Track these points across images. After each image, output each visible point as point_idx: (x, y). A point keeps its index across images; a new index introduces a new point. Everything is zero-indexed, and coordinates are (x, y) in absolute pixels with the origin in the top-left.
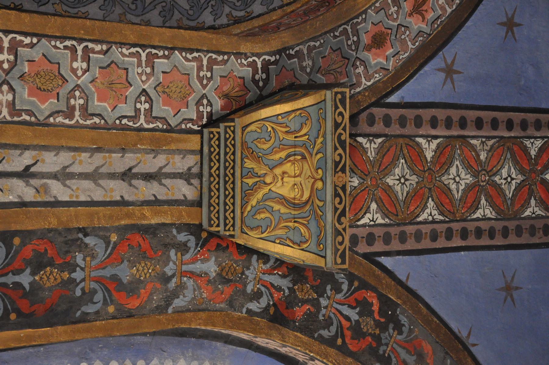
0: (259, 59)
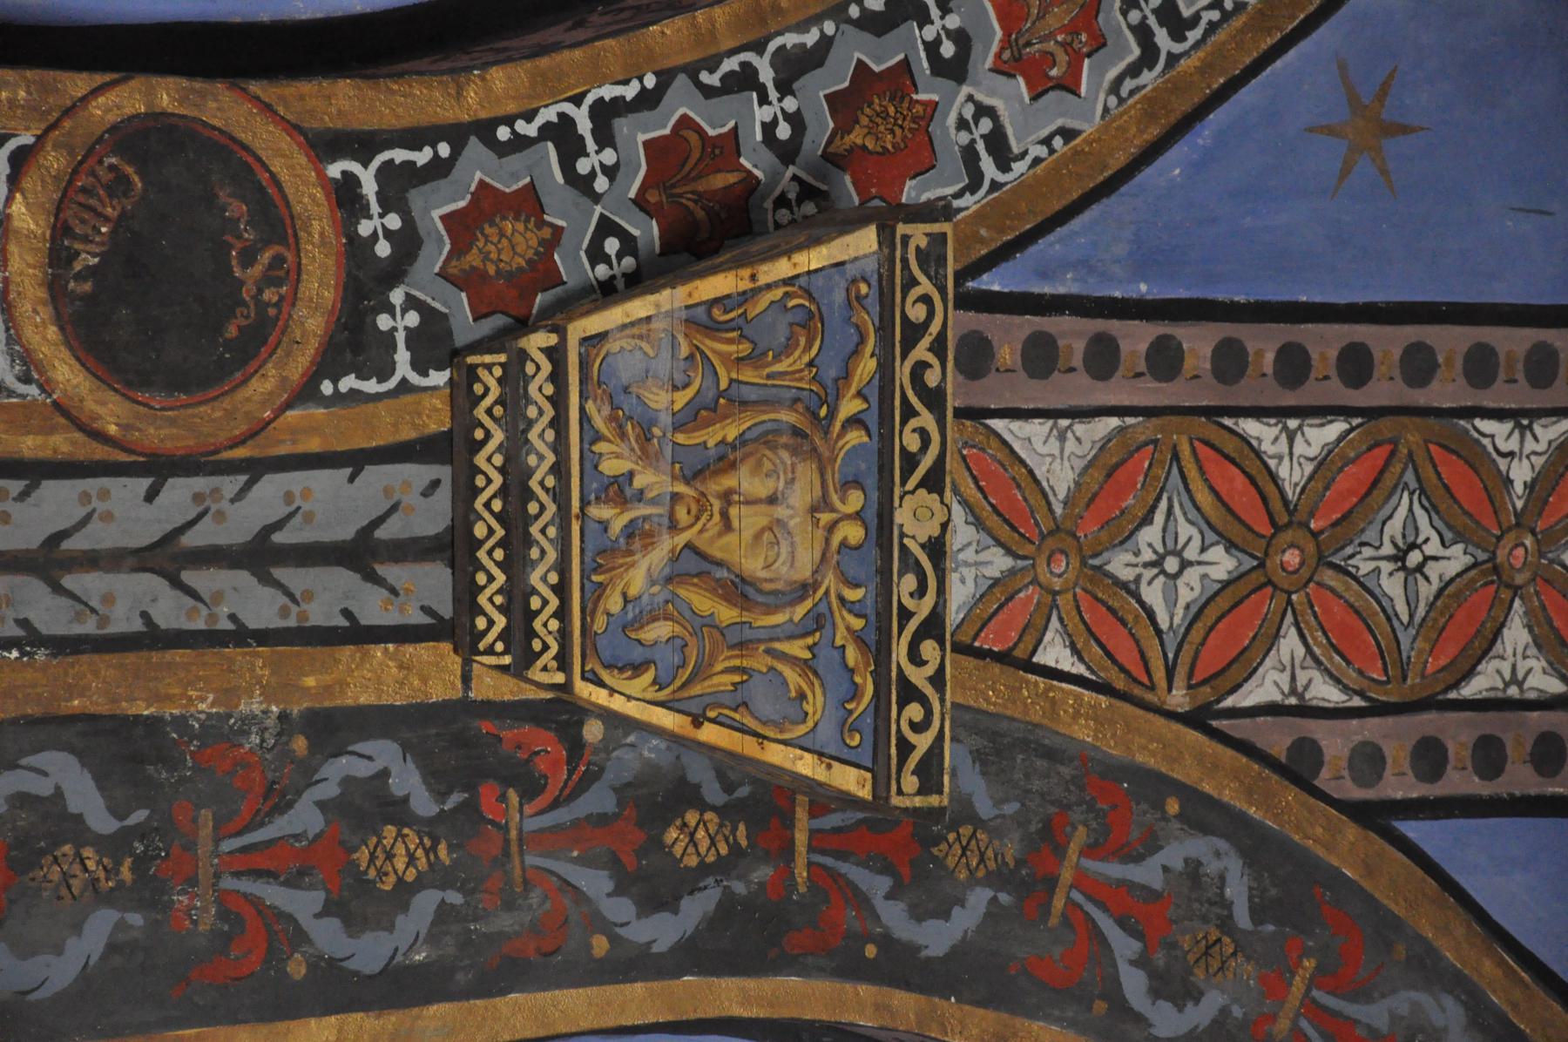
0: (365, 166)
